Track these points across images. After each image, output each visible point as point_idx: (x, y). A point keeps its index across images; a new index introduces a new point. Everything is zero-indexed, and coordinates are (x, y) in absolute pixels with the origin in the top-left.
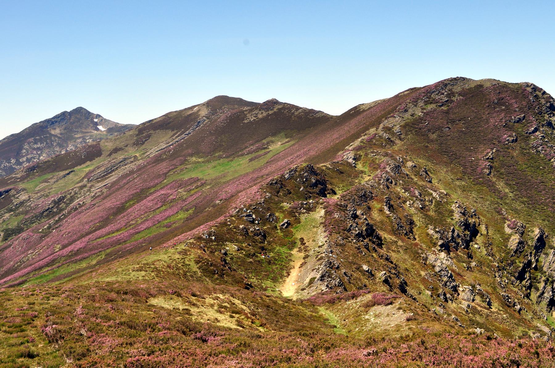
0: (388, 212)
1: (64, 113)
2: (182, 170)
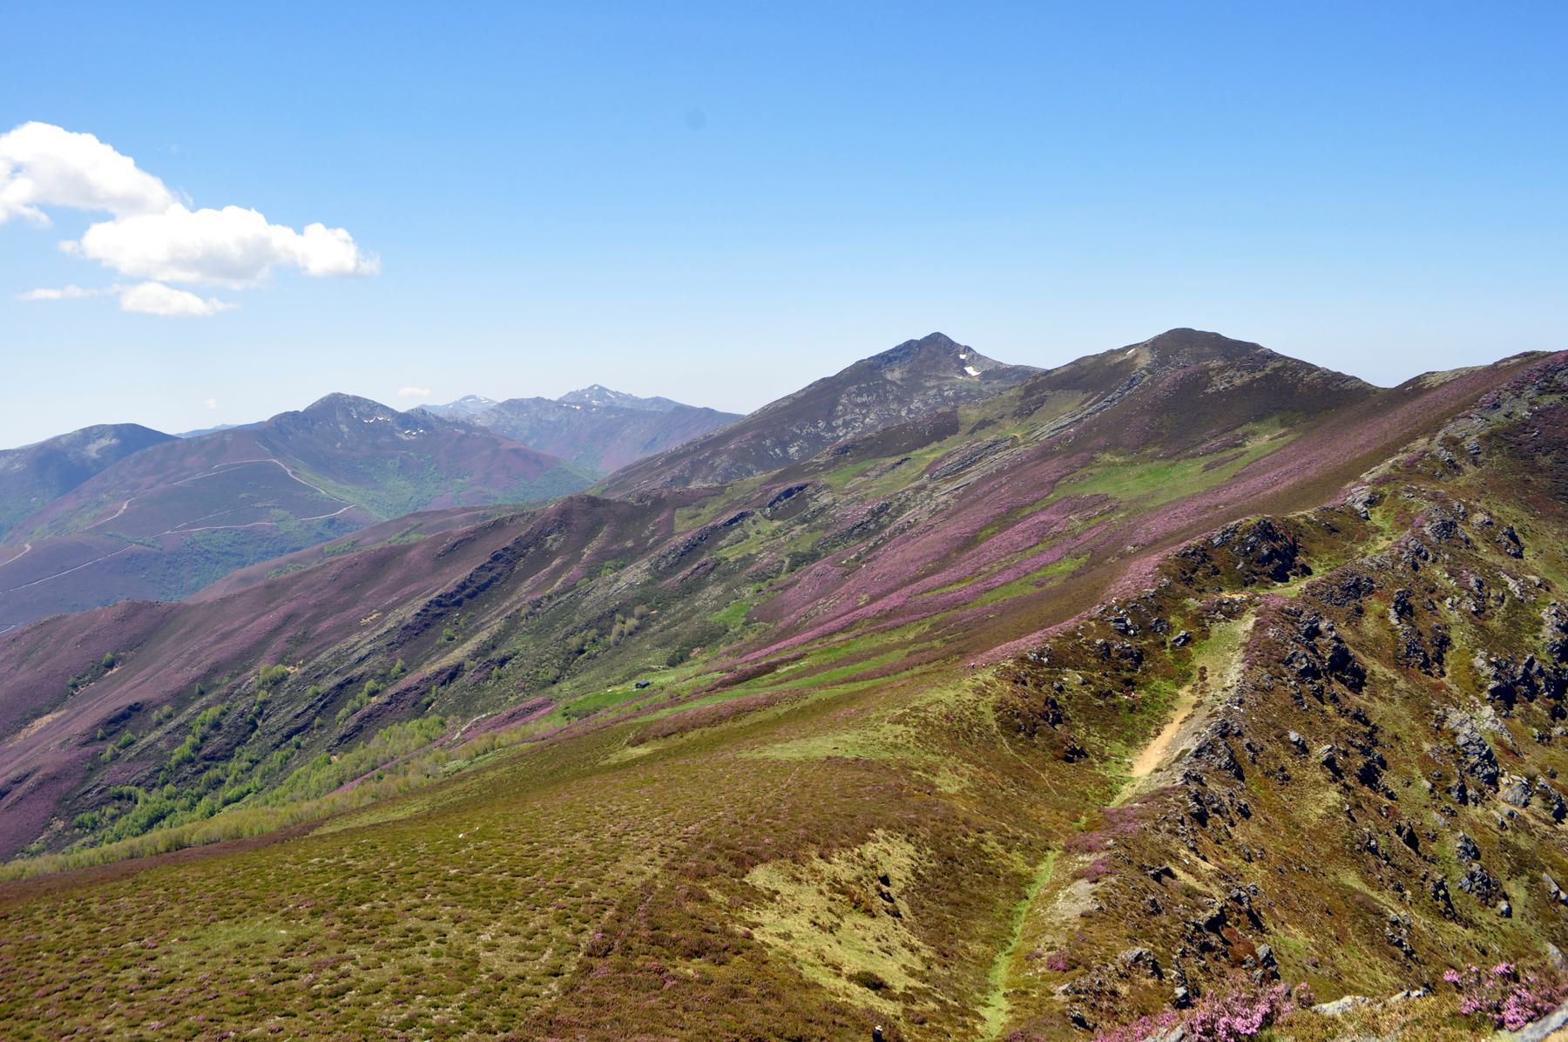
0: (1394, 621)
1: (909, 344)
2: (1083, 477)
